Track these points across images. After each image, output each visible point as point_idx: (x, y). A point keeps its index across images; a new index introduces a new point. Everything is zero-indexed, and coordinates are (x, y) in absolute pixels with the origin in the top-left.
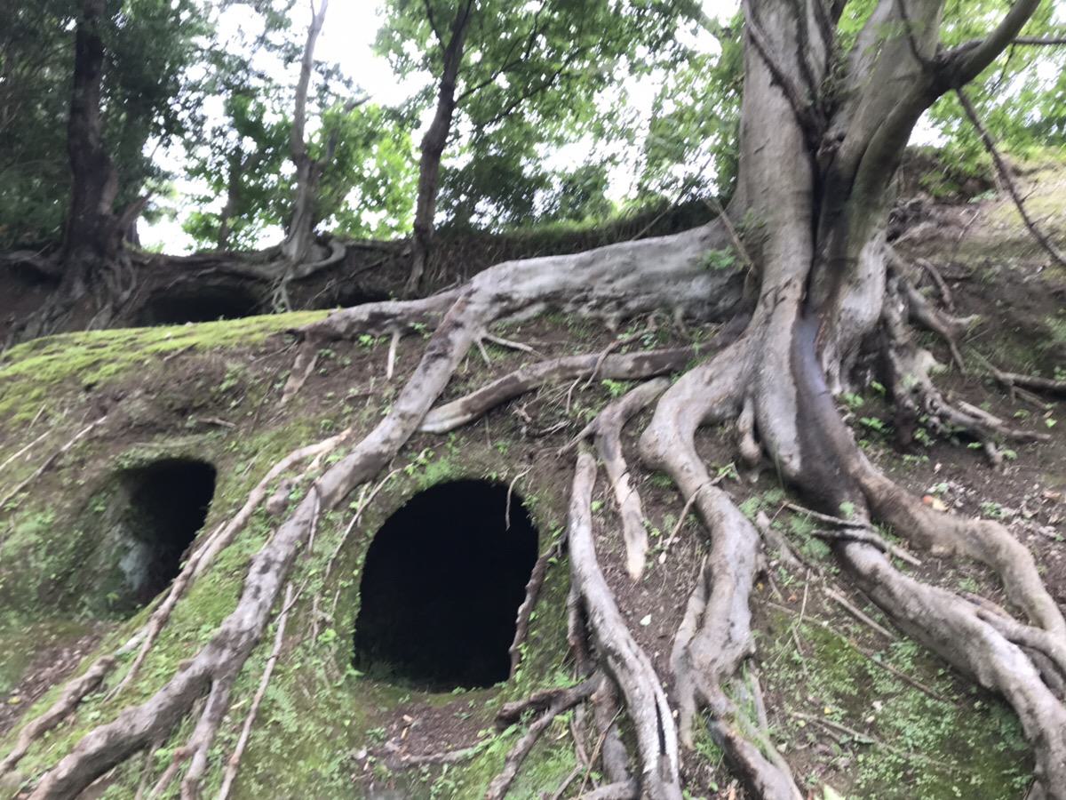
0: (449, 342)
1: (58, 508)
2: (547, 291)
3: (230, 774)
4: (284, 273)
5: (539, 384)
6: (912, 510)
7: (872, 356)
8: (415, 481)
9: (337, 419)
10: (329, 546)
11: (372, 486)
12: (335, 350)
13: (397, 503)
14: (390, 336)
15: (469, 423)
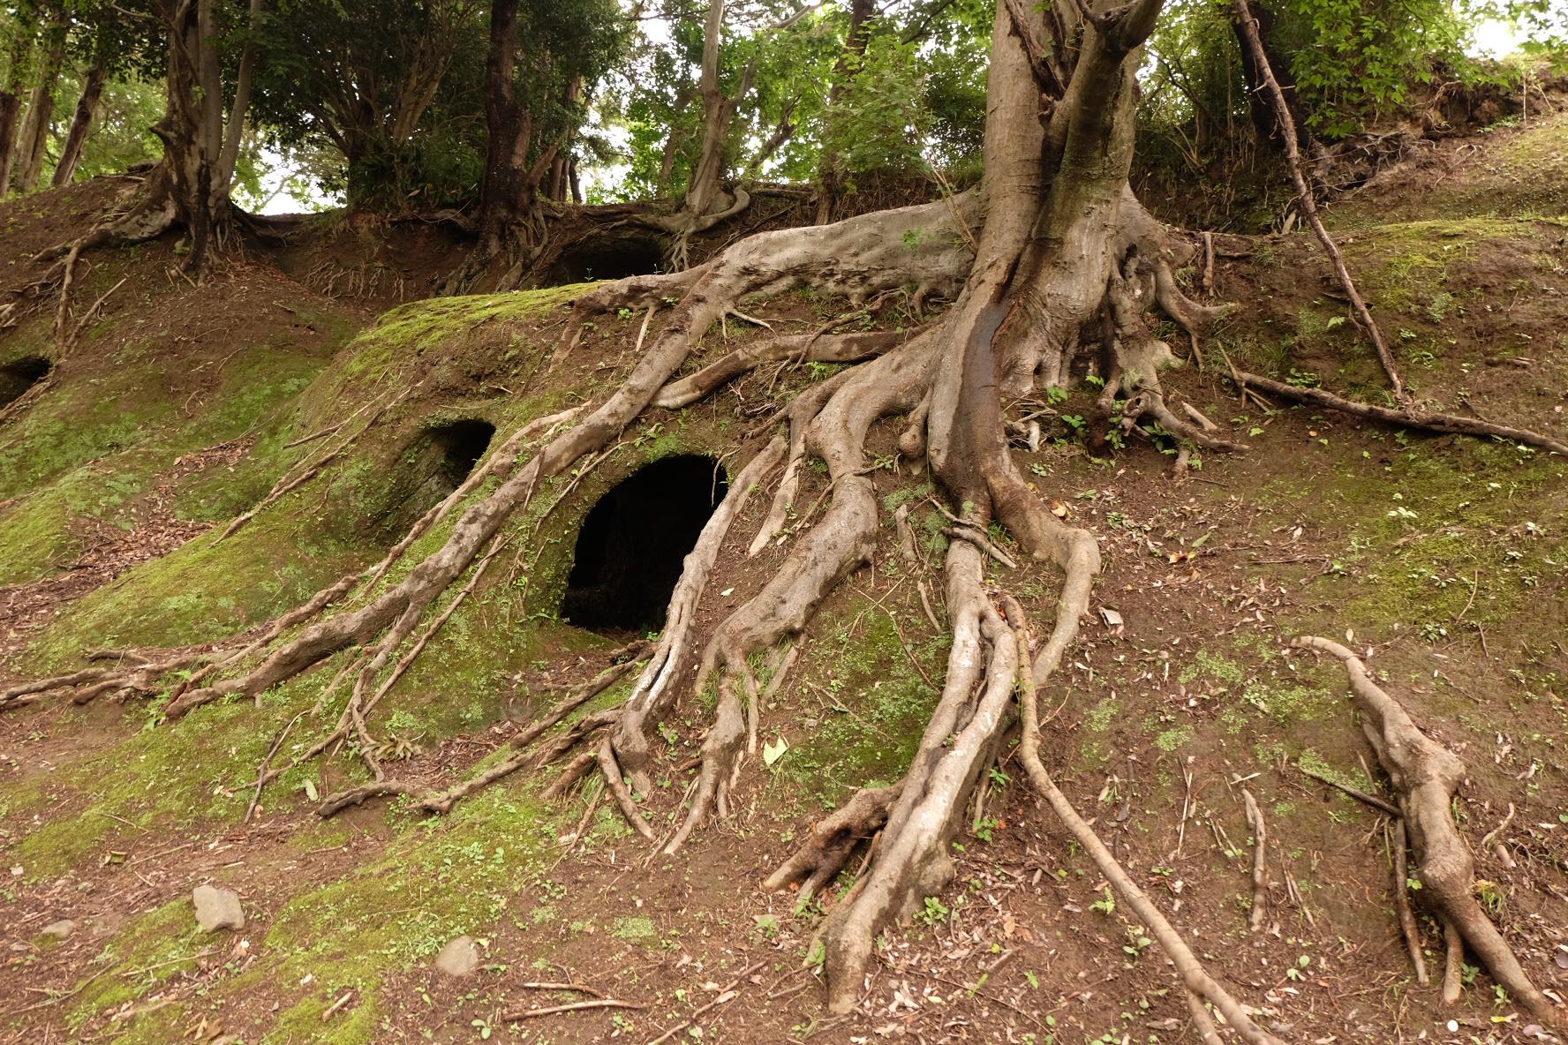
0: (688, 318)
1: (376, 458)
2: (795, 264)
3: (398, 671)
4: (686, 224)
5: (755, 363)
6: (1029, 514)
7: (1094, 347)
8: (643, 454)
9: (581, 391)
10: (543, 507)
11: (598, 456)
12: (598, 323)
13: (621, 473)
14: (646, 309)
15: (700, 400)
